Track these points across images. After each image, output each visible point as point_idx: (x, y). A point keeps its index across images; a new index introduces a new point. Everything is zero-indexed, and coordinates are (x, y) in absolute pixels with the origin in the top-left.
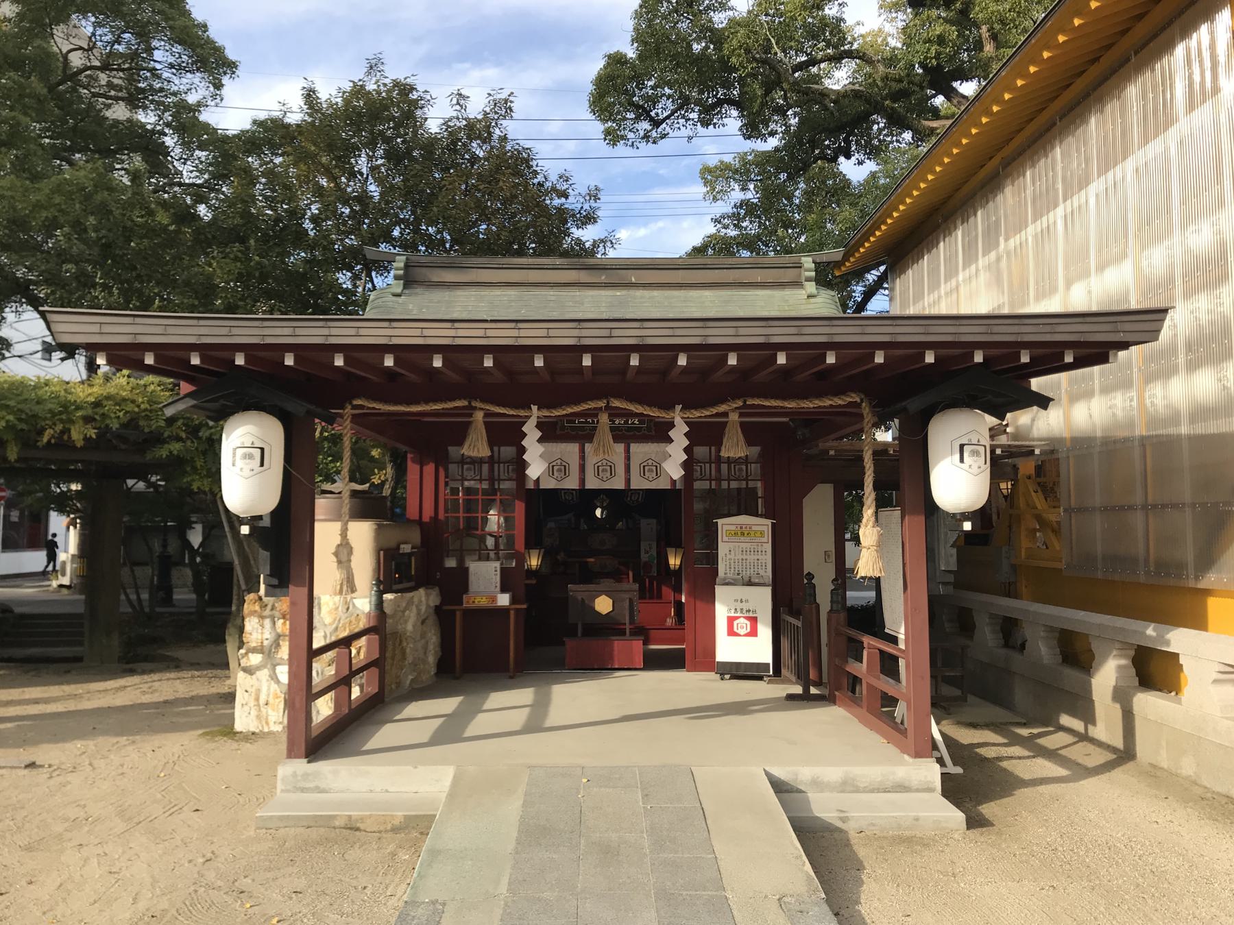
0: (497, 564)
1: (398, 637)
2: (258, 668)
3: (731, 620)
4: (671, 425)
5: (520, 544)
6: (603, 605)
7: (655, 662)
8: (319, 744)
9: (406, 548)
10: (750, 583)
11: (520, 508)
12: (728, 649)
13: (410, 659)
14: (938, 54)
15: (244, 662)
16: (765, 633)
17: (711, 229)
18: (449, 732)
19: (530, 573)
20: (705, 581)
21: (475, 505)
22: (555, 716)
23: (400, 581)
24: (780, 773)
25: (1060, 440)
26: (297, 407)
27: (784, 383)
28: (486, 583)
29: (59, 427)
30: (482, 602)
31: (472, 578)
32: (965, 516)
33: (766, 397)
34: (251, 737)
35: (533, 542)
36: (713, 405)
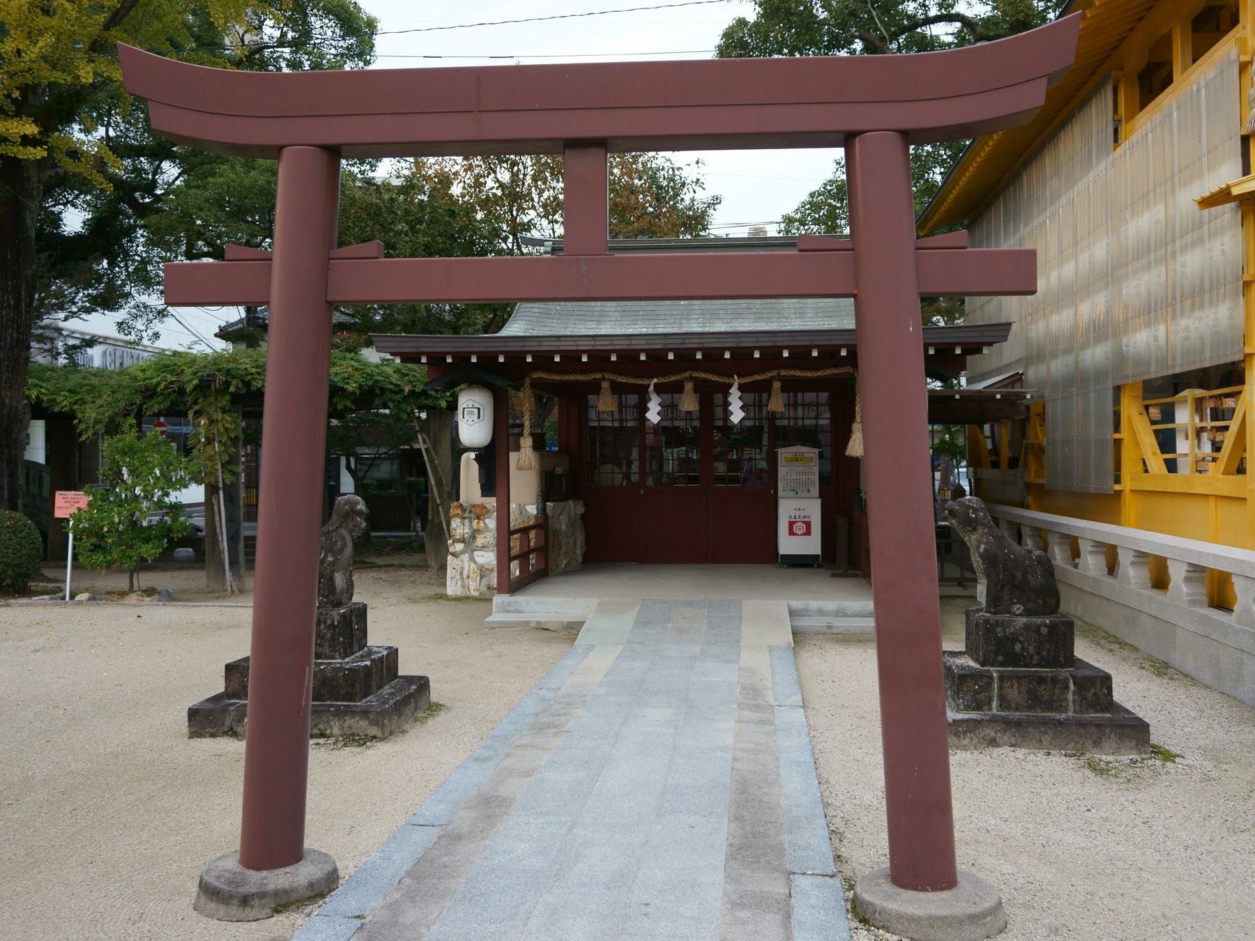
3: (791, 524)
4: (730, 386)
8: (513, 587)
9: (559, 470)
12: (788, 545)
15: (451, 549)
26: (500, 382)
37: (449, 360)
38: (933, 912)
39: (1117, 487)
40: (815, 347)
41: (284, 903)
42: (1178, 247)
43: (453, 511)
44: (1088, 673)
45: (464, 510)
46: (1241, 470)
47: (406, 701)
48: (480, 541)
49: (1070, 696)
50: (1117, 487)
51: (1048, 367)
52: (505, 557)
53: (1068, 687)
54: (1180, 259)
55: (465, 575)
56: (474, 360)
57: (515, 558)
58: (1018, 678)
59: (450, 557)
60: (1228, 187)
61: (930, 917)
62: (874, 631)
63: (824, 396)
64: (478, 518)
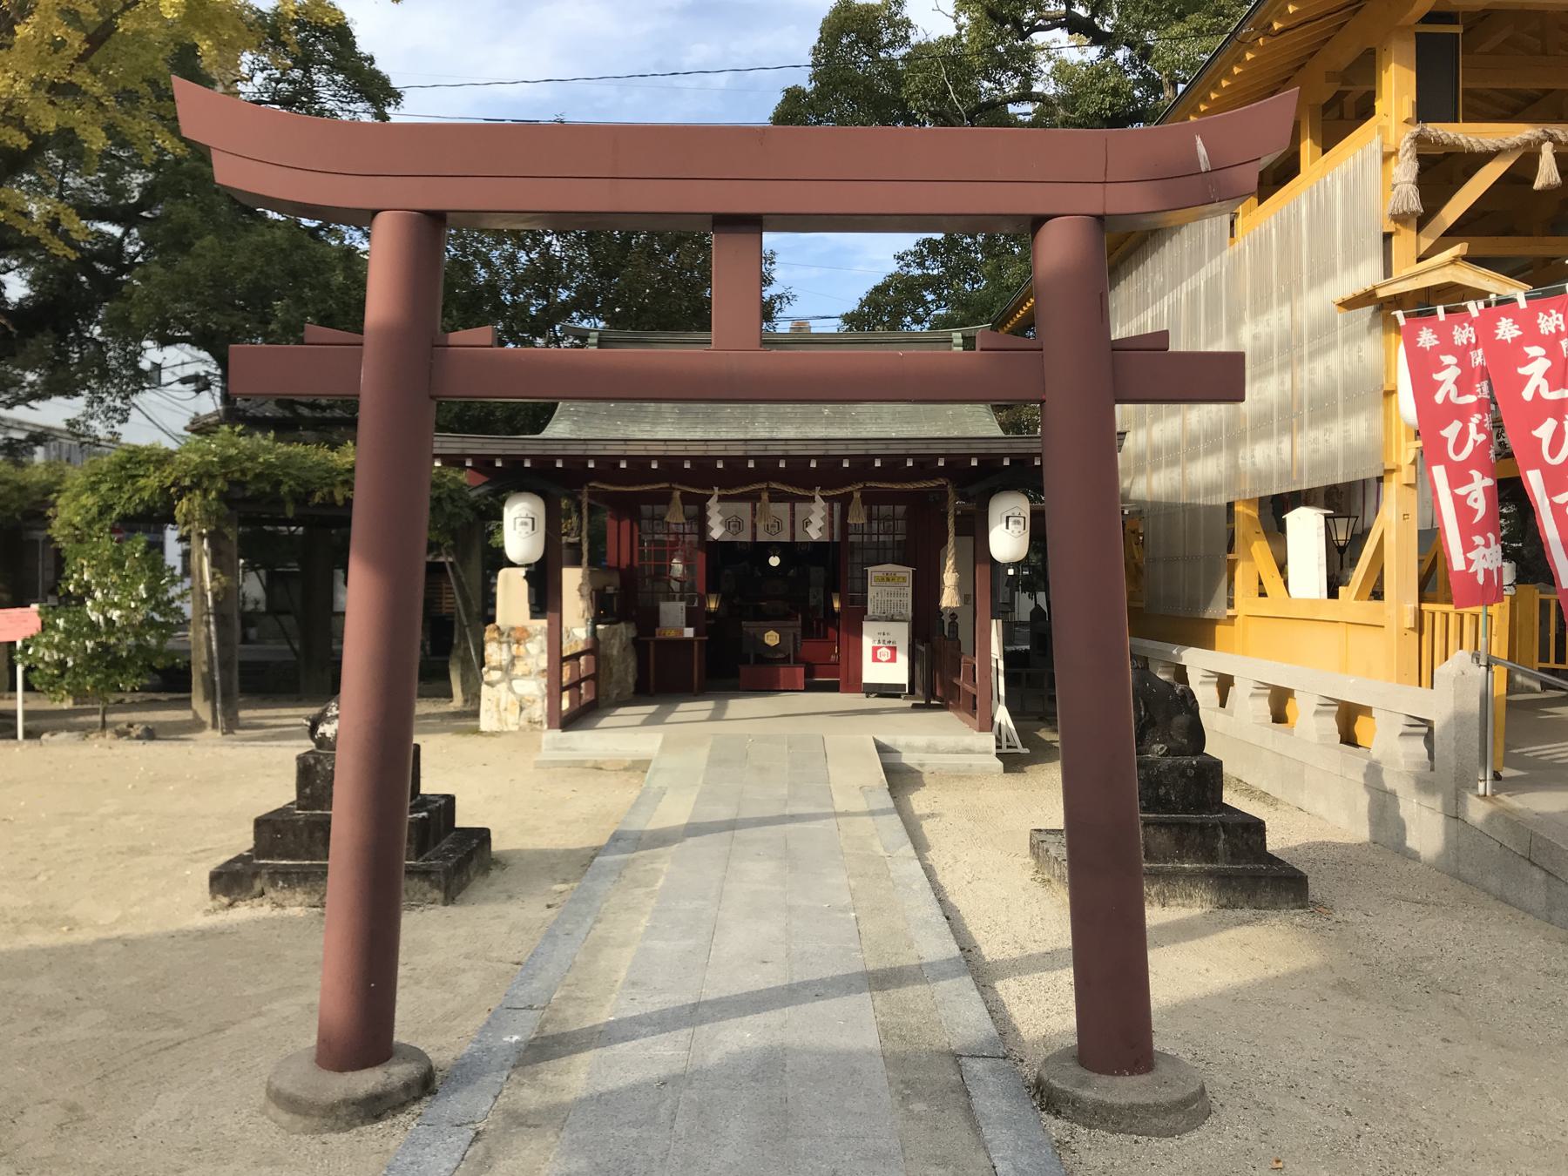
0: (683, 604)
1: (607, 658)
2: (498, 682)
3: (875, 649)
5: (701, 586)
6: (772, 638)
7: (811, 687)
8: (569, 722)
9: (610, 590)
10: (892, 620)
11: (700, 558)
12: (873, 673)
13: (615, 677)
14: (1112, 106)
15: (486, 678)
16: (903, 659)
17: (893, 267)
18: (651, 721)
19: (710, 615)
20: (856, 616)
21: (663, 554)
22: (730, 713)
23: (605, 615)
24: (884, 739)
25: (1145, 502)
27: (879, 475)
28: (675, 620)
29: (326, 490)
30: (672, 634)
31: (662, 616)
32: (1009, 565)
33: (880, 481)
34: (493, 734)
35: (712, 586)
36: (843, 486)
37: (499, 464)
38: (1136, 1100)
39: (1230, 612)
40: (910, 456)
41: (375, 1108)
42: (1306, 352)
43: (487, 635)
44: (1239, 819)
45: (501, 634)
46: (1378, 594)
47: (469, 856)
48: (520, 668)
49: (1220, 845)
50: (1230, 612)
51: (1149, 483)
52: (555, 689)
53: (1218, 836)
54: (1306, 366)
55: (502, 706)
56: (527, 464)
57: (567, 688)
58: (1160, 824)
59: (484, 688)
60: (1375, 288)
61: (1131, 1107)
62: (415, 728)
63: (900, 509)
64: (518, 642)
